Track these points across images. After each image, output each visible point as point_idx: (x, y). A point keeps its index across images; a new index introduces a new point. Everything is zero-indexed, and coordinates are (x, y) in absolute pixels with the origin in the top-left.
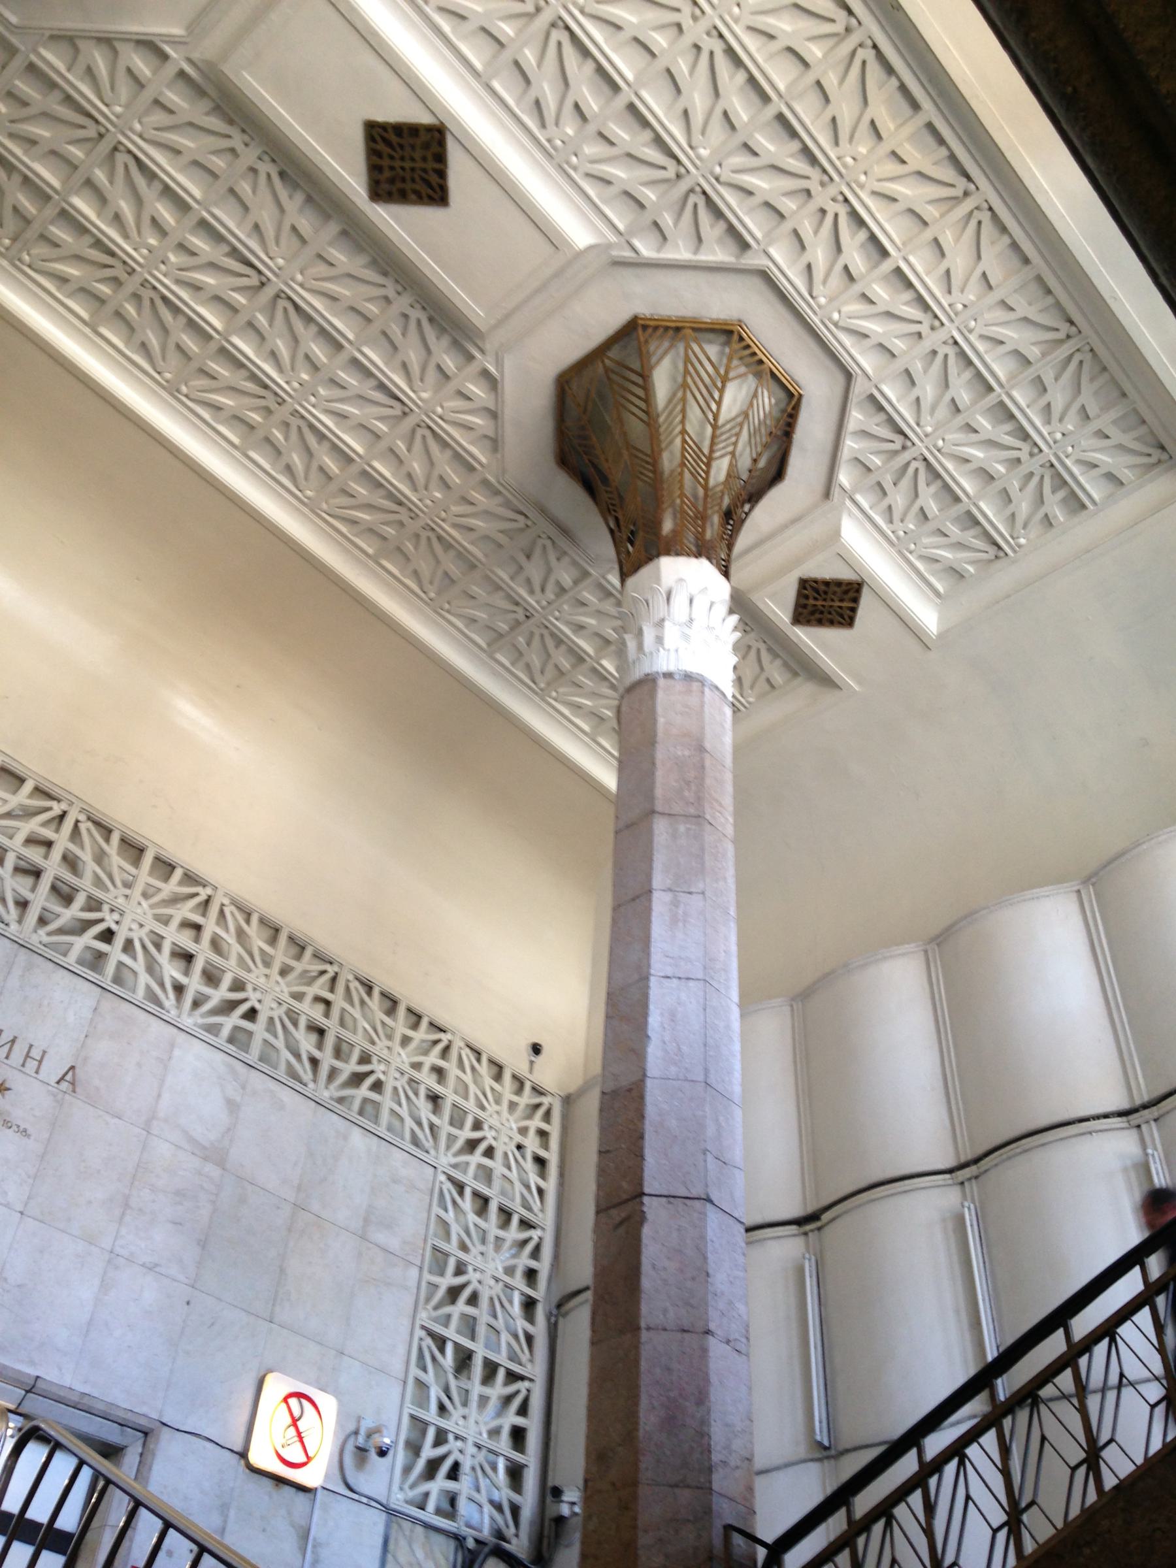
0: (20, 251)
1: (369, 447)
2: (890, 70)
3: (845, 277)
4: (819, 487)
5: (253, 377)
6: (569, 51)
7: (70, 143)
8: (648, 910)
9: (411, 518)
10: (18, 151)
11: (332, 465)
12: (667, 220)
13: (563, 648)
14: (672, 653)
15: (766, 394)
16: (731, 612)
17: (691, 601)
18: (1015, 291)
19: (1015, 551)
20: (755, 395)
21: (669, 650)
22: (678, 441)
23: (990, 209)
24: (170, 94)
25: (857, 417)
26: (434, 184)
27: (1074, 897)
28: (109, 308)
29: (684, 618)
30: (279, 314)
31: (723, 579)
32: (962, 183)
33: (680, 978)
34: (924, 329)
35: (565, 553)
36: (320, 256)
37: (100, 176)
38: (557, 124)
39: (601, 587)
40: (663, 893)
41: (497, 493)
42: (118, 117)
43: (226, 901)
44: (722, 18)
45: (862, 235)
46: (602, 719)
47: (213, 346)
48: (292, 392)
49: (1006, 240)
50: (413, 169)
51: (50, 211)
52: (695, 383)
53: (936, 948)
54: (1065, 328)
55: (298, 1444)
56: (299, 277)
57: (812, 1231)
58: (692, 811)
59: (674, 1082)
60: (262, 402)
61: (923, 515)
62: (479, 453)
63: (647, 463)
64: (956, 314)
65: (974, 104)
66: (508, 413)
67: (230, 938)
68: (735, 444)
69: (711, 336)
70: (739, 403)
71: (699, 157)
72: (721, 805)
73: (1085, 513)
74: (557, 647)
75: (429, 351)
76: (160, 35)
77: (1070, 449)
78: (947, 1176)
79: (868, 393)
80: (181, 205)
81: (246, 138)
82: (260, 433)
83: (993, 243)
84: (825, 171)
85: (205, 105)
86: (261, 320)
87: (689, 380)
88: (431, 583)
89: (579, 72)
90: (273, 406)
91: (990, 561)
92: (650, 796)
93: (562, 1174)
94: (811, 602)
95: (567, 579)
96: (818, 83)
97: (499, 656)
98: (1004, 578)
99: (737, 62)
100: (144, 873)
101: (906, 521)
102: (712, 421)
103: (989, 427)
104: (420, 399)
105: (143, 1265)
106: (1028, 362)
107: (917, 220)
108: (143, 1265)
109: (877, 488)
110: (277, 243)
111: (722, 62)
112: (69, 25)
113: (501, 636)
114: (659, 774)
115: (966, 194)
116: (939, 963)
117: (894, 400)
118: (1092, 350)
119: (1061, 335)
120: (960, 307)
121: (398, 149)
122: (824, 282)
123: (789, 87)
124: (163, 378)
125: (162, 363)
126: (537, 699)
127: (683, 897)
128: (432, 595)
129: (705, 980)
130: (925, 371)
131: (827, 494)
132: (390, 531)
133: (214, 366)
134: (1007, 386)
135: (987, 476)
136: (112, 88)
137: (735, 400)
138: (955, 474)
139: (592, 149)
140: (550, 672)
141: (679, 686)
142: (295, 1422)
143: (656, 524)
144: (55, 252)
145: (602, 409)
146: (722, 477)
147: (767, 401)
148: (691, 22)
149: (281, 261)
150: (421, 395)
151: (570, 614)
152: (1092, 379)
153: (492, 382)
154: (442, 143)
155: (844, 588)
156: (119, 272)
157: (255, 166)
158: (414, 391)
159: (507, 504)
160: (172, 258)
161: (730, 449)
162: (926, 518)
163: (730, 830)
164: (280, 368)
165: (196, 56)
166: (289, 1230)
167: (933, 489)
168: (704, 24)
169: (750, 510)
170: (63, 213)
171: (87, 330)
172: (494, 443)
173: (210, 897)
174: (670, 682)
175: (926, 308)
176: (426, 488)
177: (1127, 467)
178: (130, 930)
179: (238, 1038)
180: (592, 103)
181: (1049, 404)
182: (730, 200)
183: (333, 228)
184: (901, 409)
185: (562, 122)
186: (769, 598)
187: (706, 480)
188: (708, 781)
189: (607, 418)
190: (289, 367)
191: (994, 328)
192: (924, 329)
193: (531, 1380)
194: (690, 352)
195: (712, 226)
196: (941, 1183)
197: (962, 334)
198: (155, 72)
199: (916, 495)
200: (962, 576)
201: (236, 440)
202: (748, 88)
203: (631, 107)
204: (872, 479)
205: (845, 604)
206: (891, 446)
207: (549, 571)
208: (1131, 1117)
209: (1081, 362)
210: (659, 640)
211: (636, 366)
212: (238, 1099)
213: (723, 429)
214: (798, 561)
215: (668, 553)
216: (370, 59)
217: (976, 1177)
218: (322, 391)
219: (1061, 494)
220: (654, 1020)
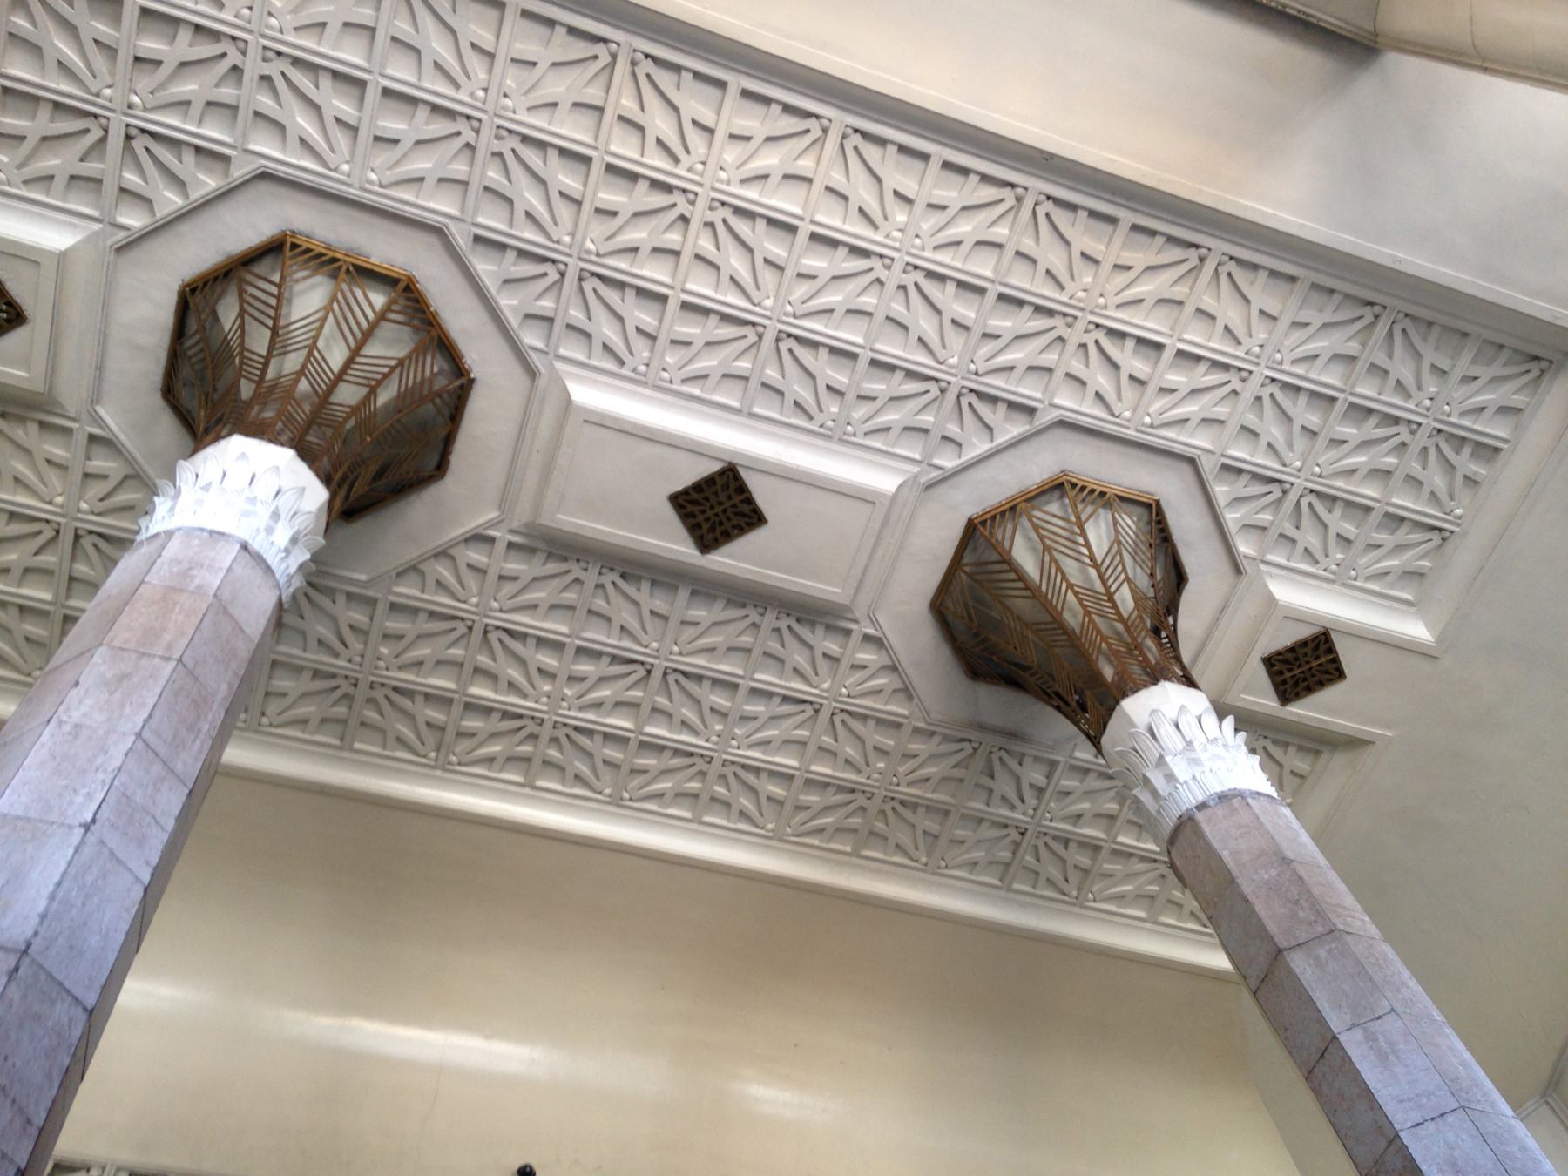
0: (447, 755)
1: (801, 757)
2: (1073, 207)
3: (1137, 385)
4: (1225, 567)
5: (677, 752)
6: (801, 352)
7: (449, 647)
8: (1346, 1058)
9: (869, 799)
10: (411, 677)
12: (953, 429)
15: (1125, 517)
17: (1177, 727)
18: (1300, 308)
19: (1458, 525)
20: (1115, 523)
21: (1185, 782)
22: (1070, 595)
23: (1231, 258)
24: (509, 566)
25: (1222, 491)
26: (748, 512)
28: (537, 762)
29: (1180, 745)
30: (674, 688)
31: (1192, 691)
32: (1193, 255)
33: (1433, 1119)
34: (1236, 384)
35: (1023, 755)
36: (683, 623)
37: (483, 660)
39: (1073, 768)
40: (1348, 1033)
41: (933, 733)
42: (477, 606)
44: (909, 254)
45: (1130, 344)
46: (1152, 897)
47: (633, 745)
48: (715, 747)
51: (457, 709)
52: (1056, 542)
54: (1368, 313)
56: (676, 649)
60: (694, 770)
61: (1344, 540)
62: (898, 708)
63: (1055, 629)
64: (1258, 357)
65: (1163, 187)
66: (904, 660)
68: (1124, 569)
69: (1045, 498)
70: (1104, 537)
71: (951, 367)
72: (1345, 908)
75: (810, 647)
76: (481, 526)
77: (1446, 407)
79: (1219, 464)
80: (557, 646)
81: (583, 564)
82: (705, 797)
83: (1252, 283)
84: (1065, 315)
85: (539, 558)
86: (662, 701)
87: (1049, 542)
88: (917, 849)
89: (820, 363)
90: (704, 767)
91: (1440, 546)
92: (1264, 935)
94: (1288, 675)
95: (1038, 777)
96: (1018, 253)
97: (1016, 886)
98: (1465, 555)
99: (941, 278)
101: (1330, 554)
103: (1355, 431)
104: (822, 690)
106: (1352, 359)
109: (1282, 540)
111: (929, 287)
112: (408, 557)
113: (1008, 865)
115: (1202, 260)
117: (1247, 457)
118: (1407, 315)
119: (1369, 319)
120: (1257, 349)
121: (706, 503)
122: (1120, 399)
123: (995, 270)
125: (598, 784)
126: (1076, 909)
127: (1375, 1026)
128: (924, 859)
130: (1261, 419)
131: (1238, 570)
132: (856, 821)
133: (642, 762)
134: (1347, 388)
135: (1385, 474)
136: (463, 588)
137: (1100, 537)
138: (1349, 488)
140: (1074, 877)
141: (1220, 811)
143: (1098, 676)
144: (475, 741)
146: (1131, 604)
147: (1129, 523)
149: (655, 645)
150: (822, 688)
151: (1062, 809)
153: (877, 642)
154: (742, 489)
155: (1312, 645)
156: (532, 727)
157: (600, 582)
158: (816, 688)
159: (946, 739)
160: (568, 692)
161: (1123, 576)
162: (1348, 541)
163: (1373, 930)
164: (694, 732)
165: (515, 525)
167: (1338, 512)
168: (897, 268)
169: (1175, 620)
170: (468, 706)
171: (527, 791)
172: (907, 692)
174: (1207, 812)
175: (1226, 367)
177: (1514, 394)
180: (840, 378)
181: (1398, 382)
182: (996, 384)
183: (683, 594)
184: (1260, 461)
185: (824, 407)
186: (1243, 692)
187: (1118, 613)
188: (1316, 891)
189: (994, 614)
190: (702, 727)
191: (1302, 348)
192: (1236, 384)
194: (1034, 520)
198: (490, 556)
199: (1325, 526)
200: (1422, 575)
201: (687, 815)
202: (961, 292)
203: (874, 363)
204: (1272, 534)
205: (1323, 660)
206: (1270, 498)
207: (1018, 780)
209: (1404, 330)
210: (1170, 777)
211: (995, 557)
213: (1105, 565)
214: (1251, 644)
215: (1124, 695)
216: (648, 449)
218: (738, 732)
219: (1467, 451)
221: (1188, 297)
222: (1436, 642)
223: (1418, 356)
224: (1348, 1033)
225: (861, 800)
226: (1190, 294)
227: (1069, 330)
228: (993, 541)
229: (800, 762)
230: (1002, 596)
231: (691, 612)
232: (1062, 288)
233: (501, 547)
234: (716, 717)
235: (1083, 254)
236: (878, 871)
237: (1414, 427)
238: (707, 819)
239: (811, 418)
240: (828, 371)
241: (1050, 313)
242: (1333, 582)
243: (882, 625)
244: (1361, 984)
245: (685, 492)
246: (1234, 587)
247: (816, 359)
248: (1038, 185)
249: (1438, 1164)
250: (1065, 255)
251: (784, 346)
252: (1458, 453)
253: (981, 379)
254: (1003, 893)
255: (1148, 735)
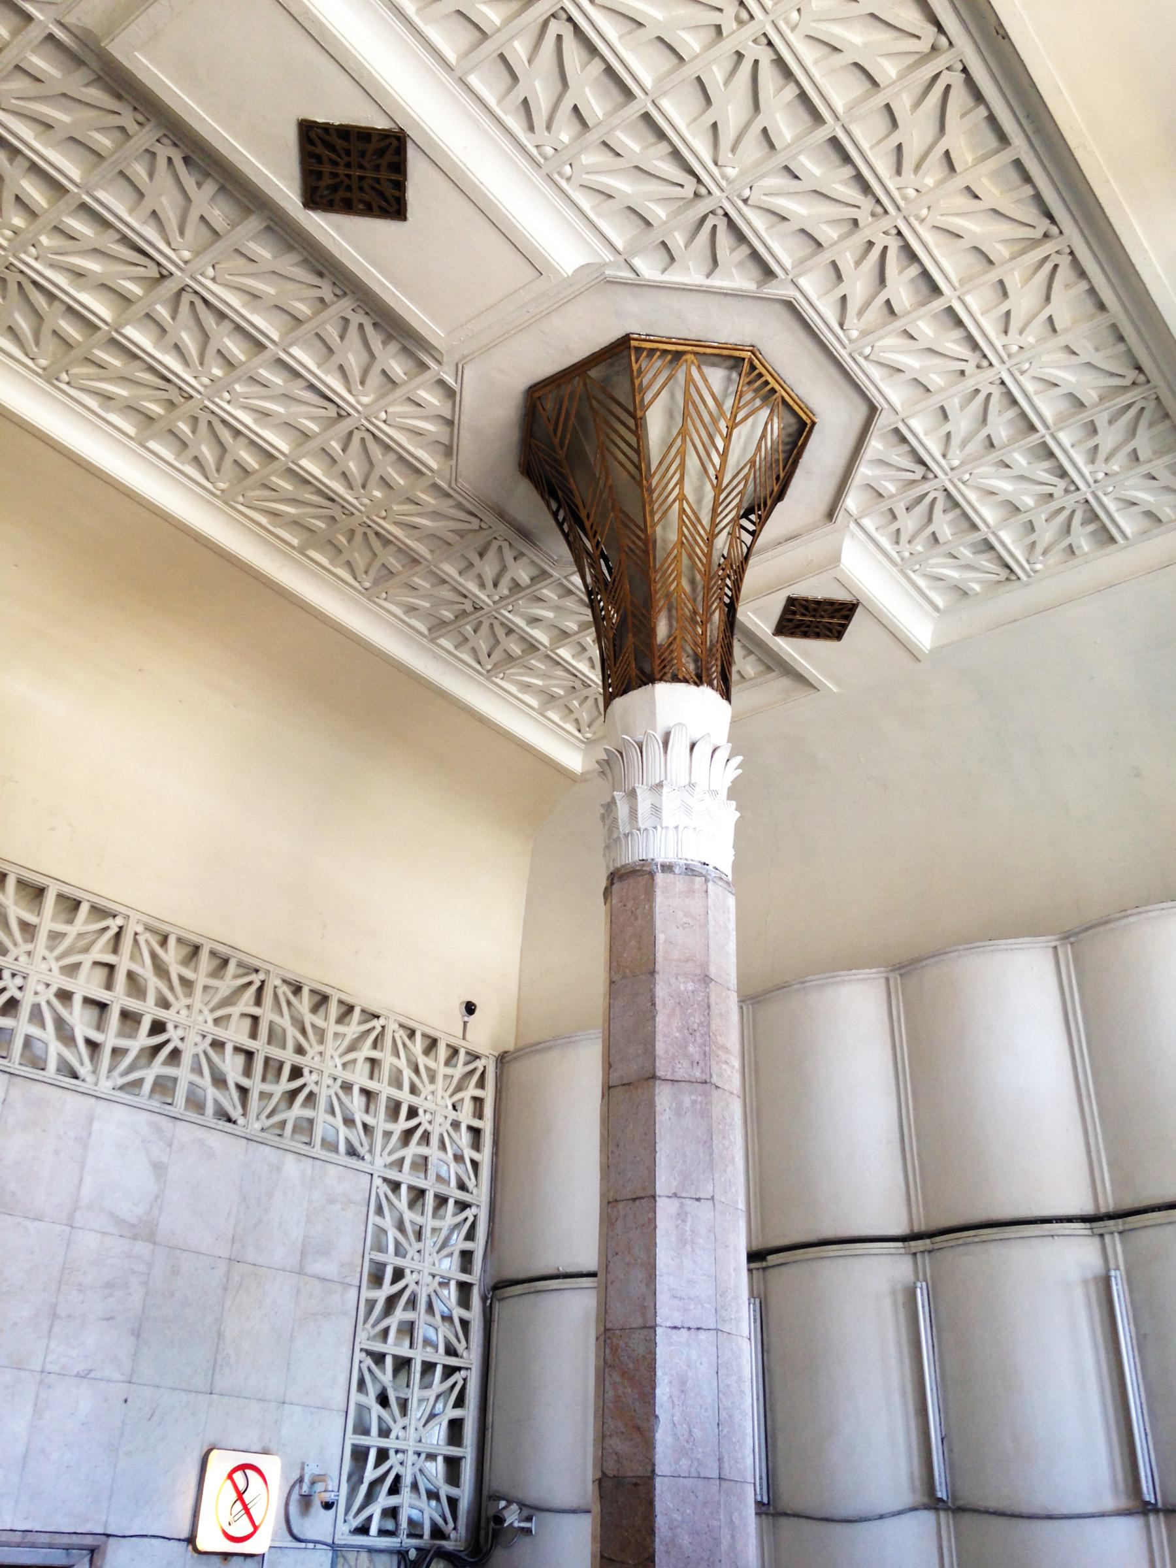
2: (978, 97)
4: (822, 507)
6: (571, 46)
8: (651, 1225)
11: (250, 460)
12: (678, 240)
13: (513, 637)
14: (672, 832)
16: (728, 742)
17: (693, 746)
19: (1029, 576)
21: (667, 828)
25: (876, 445)
27: (1050, 953)
29: (684, 780)
30: (184, 308)
31: (725, 702)
32: (1044, 225)
33: (689, 1329)
35: (522, 554)
38: (549, 128)
41: (448, 495)
43: (140, 929)
49: (1084, 286)
50: (361, 178)
53: (899, 978)
54: (1132, 375)
55: (245, 1517)
57: (758, 1269)
58: (697, 1073)
59: (685, 1481)
64: (1009, 356)
67: (146, 971)
71: (724, 177)
73: (1113, 547)
74: (507, 635)
78: (900, 1244)
80: (56, 187)
91: (1000, 582)
93: (496, 1143)
98: (1013, 599)
100: (47, 918)
102: (713, 478)
104: (358, 402)
105: (77, 1375)
107: (980, 256)
108: (77, 1375)
110: (182, 233)
111: (768, 73)
114: (660, 1019)
116: (901, 997)
119: (1127, 382)
121: (344, 156)
122: (860, 313)
123: (850, 108)
124: (37, 365)
125: (35, 350)
126: (482, 679)
127: (691, 1205)
129: (717, 1330)
131: (830, 515)
139: (593, 158)
142: (240, 1496)
145: (580, 434)
148: (734, 25)
152: (1151, 425)
154: (399, 167)
164: (186, 362)
165: (69, 20)
166: (225, 1289)
167: (950, 516)
172: (449, 451)
173: (121, 928)
176: (364, 487)
178: (36, 993)
179: (164, 1086)
182: (756, 223)
193: (467, 1369)
195: (732, 250)
196: (893, 1251)
197: (1012, 374)
201: (131, 430)
202: (797, 103)
207: (504, 569)
208: (1094, 1225)
210: (656, 810)
212: (165, 1159)
214: (793, 580)
217: (930, 1252)
220: (662, 1392)
221: (1003, 263)
222: (931, 651)
223: (1133, 432)
224: (667, 1199)
225: (336, 512)
226: (1006, 262)
227: (870, 219)
228: (637, 382)
229: (292, 450)
230: (608, 449)
231: (252, 245)
232: (899, 172)
233: (34, 33)
234: (220, 360)
235: (947, 153)
236: (315, 575)
237: (1072, 488)
238: (152, 444)
239: (531, 128)
240: (587, 91)
241: (866, 189)
242: (895, 564)
243: (465, 381)
244: (701, 1155)
245: (326, 128)
246: (814, 527)
247: (583, 67)
248: (966, 49)
249: (672, 1375)
250: (929, 140)
251: (555, 27)
252: (1082, 524)
253: (745, 210)
254: (425, 641)
255: (661, 745)
